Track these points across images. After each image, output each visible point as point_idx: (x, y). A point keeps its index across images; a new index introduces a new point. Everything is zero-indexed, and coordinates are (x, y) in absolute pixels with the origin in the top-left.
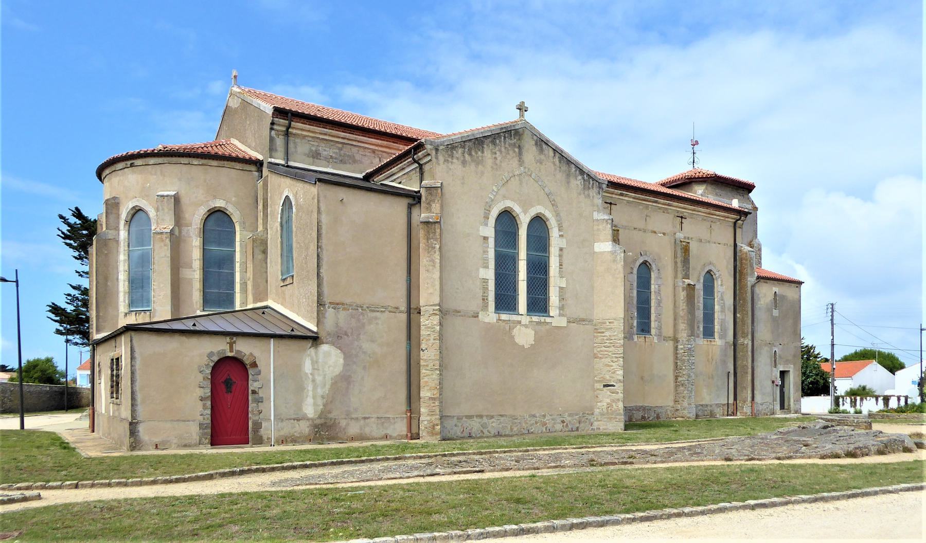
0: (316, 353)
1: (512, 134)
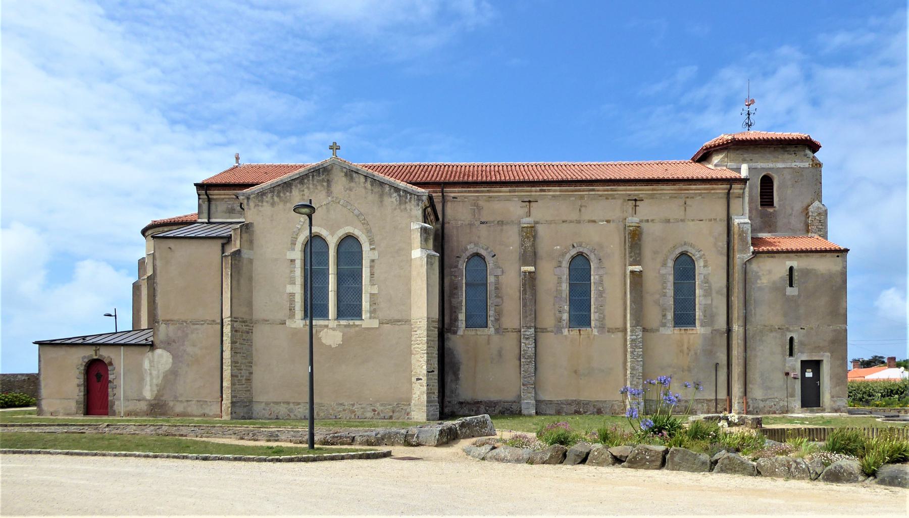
0: (153, 356)
1: (321, 172)
